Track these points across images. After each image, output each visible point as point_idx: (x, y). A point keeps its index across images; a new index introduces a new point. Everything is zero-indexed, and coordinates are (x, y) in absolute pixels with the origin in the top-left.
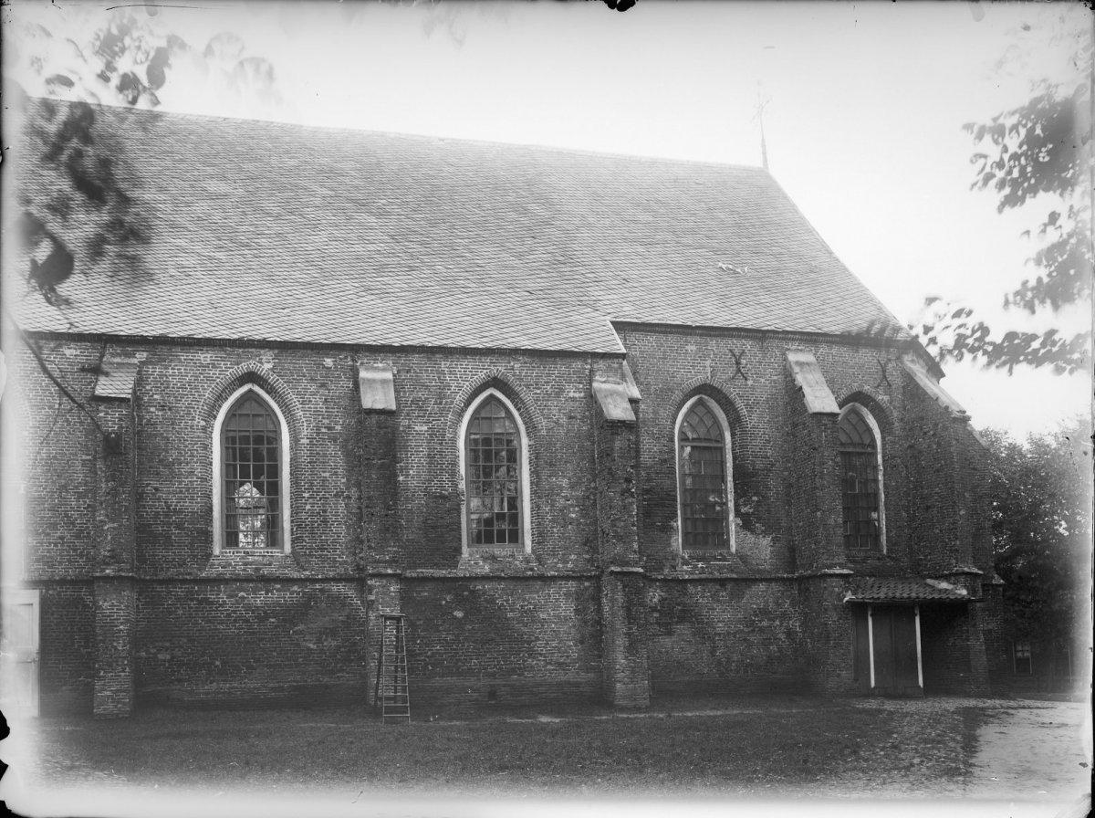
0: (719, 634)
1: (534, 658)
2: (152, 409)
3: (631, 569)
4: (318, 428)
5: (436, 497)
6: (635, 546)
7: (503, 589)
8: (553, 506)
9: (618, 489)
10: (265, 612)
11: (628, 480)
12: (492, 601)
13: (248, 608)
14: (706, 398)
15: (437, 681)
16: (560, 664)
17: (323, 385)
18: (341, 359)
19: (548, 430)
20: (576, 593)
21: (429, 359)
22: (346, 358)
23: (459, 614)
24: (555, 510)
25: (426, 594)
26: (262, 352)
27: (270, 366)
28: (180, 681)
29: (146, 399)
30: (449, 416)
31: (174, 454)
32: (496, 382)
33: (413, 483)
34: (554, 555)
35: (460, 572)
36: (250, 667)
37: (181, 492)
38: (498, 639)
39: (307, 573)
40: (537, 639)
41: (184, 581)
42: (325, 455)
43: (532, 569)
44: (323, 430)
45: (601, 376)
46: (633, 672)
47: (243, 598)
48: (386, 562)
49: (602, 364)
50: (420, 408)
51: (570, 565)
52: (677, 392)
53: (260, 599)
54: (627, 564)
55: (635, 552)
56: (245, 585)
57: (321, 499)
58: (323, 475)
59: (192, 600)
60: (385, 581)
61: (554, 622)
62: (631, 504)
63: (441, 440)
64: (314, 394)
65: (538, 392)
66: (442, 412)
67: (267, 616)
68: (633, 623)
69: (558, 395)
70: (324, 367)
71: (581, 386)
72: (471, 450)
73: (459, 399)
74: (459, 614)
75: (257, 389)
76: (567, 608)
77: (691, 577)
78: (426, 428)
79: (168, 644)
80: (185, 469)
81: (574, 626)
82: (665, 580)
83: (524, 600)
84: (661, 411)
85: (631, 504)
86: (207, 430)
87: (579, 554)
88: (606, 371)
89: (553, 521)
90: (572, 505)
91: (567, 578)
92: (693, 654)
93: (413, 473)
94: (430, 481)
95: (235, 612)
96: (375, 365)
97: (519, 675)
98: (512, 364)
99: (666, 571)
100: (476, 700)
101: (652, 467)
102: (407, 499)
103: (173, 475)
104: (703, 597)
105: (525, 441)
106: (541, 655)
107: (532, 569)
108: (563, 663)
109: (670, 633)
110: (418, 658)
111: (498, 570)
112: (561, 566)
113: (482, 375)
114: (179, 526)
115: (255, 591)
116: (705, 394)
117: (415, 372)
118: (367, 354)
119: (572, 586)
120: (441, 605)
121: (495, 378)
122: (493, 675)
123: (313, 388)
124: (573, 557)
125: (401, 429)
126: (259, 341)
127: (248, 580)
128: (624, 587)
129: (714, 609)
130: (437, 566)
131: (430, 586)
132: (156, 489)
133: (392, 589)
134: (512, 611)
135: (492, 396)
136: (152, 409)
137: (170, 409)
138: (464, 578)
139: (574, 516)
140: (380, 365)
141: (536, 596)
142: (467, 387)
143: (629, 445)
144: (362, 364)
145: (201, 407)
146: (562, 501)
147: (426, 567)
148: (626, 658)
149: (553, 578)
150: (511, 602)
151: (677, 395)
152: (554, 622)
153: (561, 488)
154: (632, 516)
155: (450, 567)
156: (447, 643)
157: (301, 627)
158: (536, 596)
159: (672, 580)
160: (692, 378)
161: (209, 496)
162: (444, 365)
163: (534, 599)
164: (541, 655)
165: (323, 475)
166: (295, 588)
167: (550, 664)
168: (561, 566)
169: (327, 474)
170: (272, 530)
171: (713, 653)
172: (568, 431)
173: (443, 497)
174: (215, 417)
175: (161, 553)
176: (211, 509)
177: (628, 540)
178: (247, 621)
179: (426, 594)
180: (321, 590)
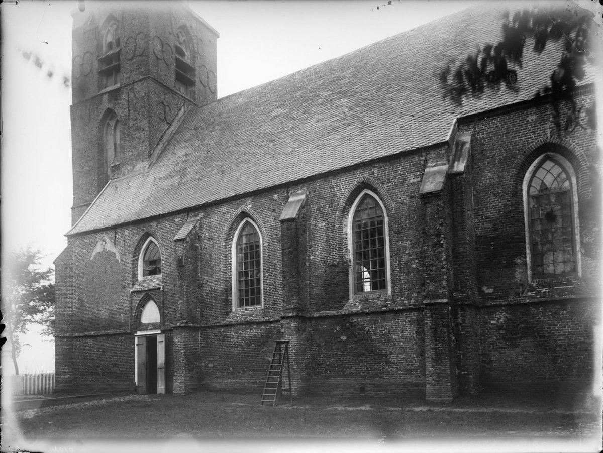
0: (560, 346)
1: (390, 366)
2: (205, 241)
3: (439, 301)
4: (272, 235)
5: (331, 266)
6: (444, 283)
8: (400, 261)
9: (430, 243)
10: (250, 341)
11: (438, 235)
12: (363, 329)
13: (243, 339)
14: (552, 154)
15: (332, 381)
16: (407, 370)
17: (274, 211)
18: (282, 193)
20: (417, 320)
21: (325, 181)
22: (284, 192)
23: (344, 338)
24: (401, 264)
26: (247, 199)
27: (250, 206)
28: (216, 377)
29: (203, 236)
30: (337, 214)
31: (213, 261)
32: (364, 185)
34: (401, 295)
36: (244, 371)
37: (216, 281)
38: (366, 353)
39: (267, 318)
40: (391, 353)
41: (217, 327)
42: (275, 251)
43: (386, 306)
44: (274, 236)
45: (432, 162)
46: (439, 376)
47: (240, 334)
49: (433, 154)
50: (321, 213)
51: (413, 301)
52: (519, 157)
53: (248, 334)
54: (438, 297)
55: (444, 288)
58: (274, 262)
59: (221, 336)
60: (288, 321)
61: (402, 341)
63: (334, 231)
65: (390, 184)
66: (333, 212)
69: (402, 183)
71: (418, 173)
72: (356, 232)
73: (342, 202)
74: (344, 338)
76: (410, 331)
77: (533, 300)
78: (324, 224)
79: (212, 359)
80: (218, 268)
81: (416, 343)
82: (509, 306)
83: (382, 327)
84: (505, 176)
85: (440, 252)
86: (227, 248)
87: (418, 293)
88: (436, 158)
89: (400, 272)
90: (413, 259)
91: (410, 310)
92: (536, 361)
93: (317, 254)
94: (327, 256)
95: (237, 341)
96: (298, 192)
97: (380, 377)
98: (373, 170)
99: (511, 298)
100: (353, 393)
101: (496, 220)
102: (315, 269)
103: (214, 273)
104: (544, 316)
105: (386, 220)
106: (394, 364)
107: (386, 306)
108: (409, 370)
109: (514, 346)
110: (322, 366)
111: (366, 308)
112: (406, 302)
113: (355, 183)
114: (216, 299)
115: (246, 330)
116: (550, 151)
117: (319, 191)
118: (294, 187)
119: (414, 315)
120: (333, 333)
121: (363, 183)
122: (364, 377)
123: (269, 213)
125: (311, 227)
126: (243, 194)
127: (241, 324)
128: (432, 314)
130: (331, 309)
131: (327, 322)
132: (207, 281)
133: (292, 325)
134: (375, 334)
136: (205, 241)
137: (212, 239)
138: (345, 315)
141: (390, 324)
142: (347, 193)
143: (438, 209)
144: (292, 193)
145: (224, 235)
146: (406, 257)
147: (325, 310)
148: (433, 366)
149: (400, 311)
150: (374, 329)
151: (520, 158)
152: (402, 341)
153: (405, 248)
154: (442, 261)
155: (338, 308)
156: (337, 356)
158: (390, 324)
159: (515, 305)
160: (532, 142)
162: (333, 182)
163: (388, 326)
164: (394, 364)
165: (274, 262)
166: (263, 327)
167: (401, 370)
168: (406, 302)
169: (276, 261)
170: (379, 283)
171: (554, 360)
172: (410, 207)
173: (334, 265)
174: (232, 239)
175: (209, 313)
177: (438, 279)
178: (242, 346)
180: (274, 328)
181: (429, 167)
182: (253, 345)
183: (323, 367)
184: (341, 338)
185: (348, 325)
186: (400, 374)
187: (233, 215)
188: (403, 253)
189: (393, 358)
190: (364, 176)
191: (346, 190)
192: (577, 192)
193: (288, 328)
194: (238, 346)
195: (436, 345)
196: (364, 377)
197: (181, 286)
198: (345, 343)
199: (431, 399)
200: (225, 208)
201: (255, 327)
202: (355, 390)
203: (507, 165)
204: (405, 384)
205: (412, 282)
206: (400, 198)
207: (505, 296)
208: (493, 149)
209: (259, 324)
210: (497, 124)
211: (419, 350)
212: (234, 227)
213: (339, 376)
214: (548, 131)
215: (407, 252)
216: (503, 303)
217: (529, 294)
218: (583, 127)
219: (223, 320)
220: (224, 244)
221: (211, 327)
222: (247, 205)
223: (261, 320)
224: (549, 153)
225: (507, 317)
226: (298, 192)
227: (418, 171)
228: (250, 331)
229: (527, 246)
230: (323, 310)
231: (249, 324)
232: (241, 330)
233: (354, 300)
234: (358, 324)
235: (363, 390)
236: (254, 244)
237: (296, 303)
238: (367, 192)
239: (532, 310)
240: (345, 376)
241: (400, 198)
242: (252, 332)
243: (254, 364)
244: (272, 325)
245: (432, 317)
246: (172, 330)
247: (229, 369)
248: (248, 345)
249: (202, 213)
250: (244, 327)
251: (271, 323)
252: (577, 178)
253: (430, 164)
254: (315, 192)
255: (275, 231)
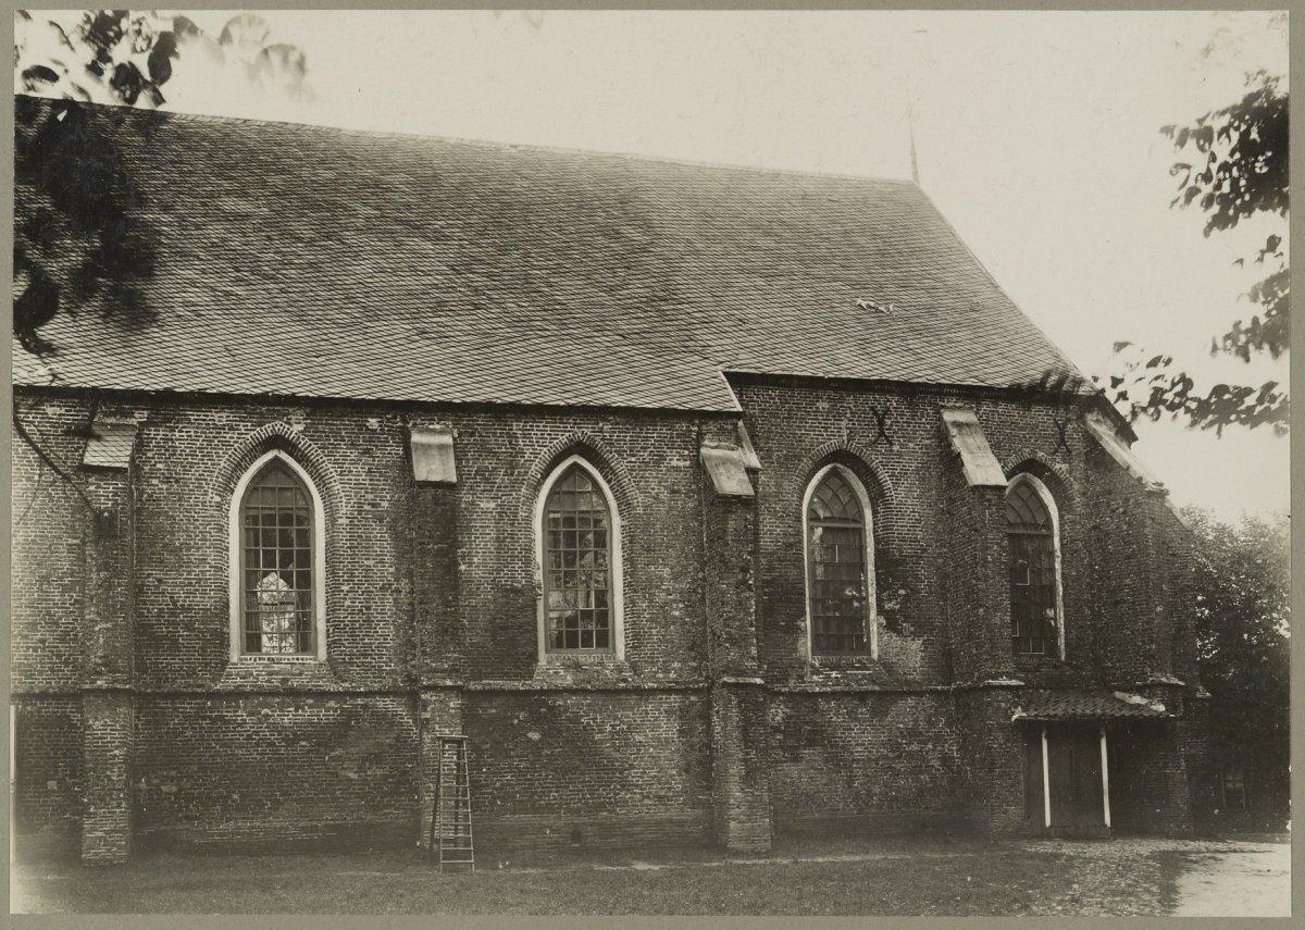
3: (749, 680)
4: (360, 505)
6: (754, 651)
7: (589, 705)
8: (651, 601)
9: (731, 581)
11: (745, 570)
12: (576, 719)
13: (274, 728)
14: (842, 467)
15: (509, 819)
16: (660, 798)
19: (646, 507)
20: (681, 709)
23: (535, 736)
25: (494, 711)
29: (147, 469)
32: (578, 447)
33: (477, 574)
35: (536, 684)
38: (583, 767)
39: (347, 685)
40: (632, 767)
41: (195, 695)
43: (625, 680)
44: (366, 507)
45: (711, 440)
48: (444, 671)
49: (712, 426)
50: (487, 481)
51: (672, 675)
53: (288, 717)
54: (742, 673)
55: (753, 658)
56: (270, 699)
57: (363, 592)
59: (204, 718)
60: (442, 694)
62: (748, 599)
64: (354, 462)
65: (633, 459)
67: (297, 738)
68: (750, 748)
69: (658, 463)
70: (367, 429)
74: (535, 736)
75: (284, 456)
76: (669, 729)
78: (492, 505)
80: (196, 555)
81: (678, 750)
85: (748, 599)
87: (683, 661)
89: (651, 620)
90: (675, 601)
91: (669, 691)
93: (478, 559)
94: (499, 571)
95: (257, 733)
96: (431, 427)
98: (601, 425)
99: (792, 683)
102: (471, 593)
103: (180, 564)
104: (837, 714)
105: (617, 521)
106: (637, 786)
108: (664, 797)
109: (796, 759)
111: (583, 681)
112: (661, 676)
114: (189, 627)
116: (841, 463)
120: (512, 724)
122: (577, 812)
124: (676, 665)
125: (463, 506)
127: (273, 693)
129: (851, 729)
130: (507, 676)
131: (499, 701)
132: (160, 581)
133: (452, 705)
135: (575, 464)
136: (155, 482)
137: (177, 482)
139: (677, 613)
140: (438, 427)
142: (545, 454)
143: (746, 526)
144: (415, 425)
149: (652, 691)
150: (603, 725)
153: (662, 579)
154: (749, 614)
155: (523, 678)
157: (338, 752)
161: (224, 590)
162: (517, 427)
163: (628, 717)
164: (637, 786)
166: (332, 704)
167: (648, 797)
168: (661, 676)
169: (371, 563)
170: (303, 632)
171: (850, 782)
174: (232, 491)
176: (227, 605)
178: (272, 744)
179: (494, 711)
180: (365, 707)
181: (707, 446)
182: (303, 743)
183: (485, 793)
184: (530, 735)
185: (543, 710)
186: (646, 805)
187: (248, 437)
188: (657, 587)
189: (634, 776)
190: (585, 431)
191: (545, 449)
192: (874, 532)
193: (442, 710)
194: (257, 745)
195: (747, 754)
196: (577, 812)
197: (107, 586)
198: (536, 747)
199: (738, 845)
200: (224, 415)
201: (311, 701)
202: (561, 837)
203: (788, 469)
204: (658, 823)
205: (673, 642)
206: (653, 489)
207: (784, 679)
208: (768, 438)
209: (321, 695)
210: (774, 399)
211: (682, 763)
212: (243, 464)
213: (525, 811)
214: (845, 432)
215: (664, 587)
216: (783, 690)
217: (815, 678)
218: (888, 441)
219: (213, 680)
220: (218, 499)
221: (175, 696)
222: (290, 425)
223: (332, 687)
224: (838, 465)
225: (786, 713)
226: (431, 427)
227: (684, 449)
228: (297, 710)
229: (807, 602)
230: (487, 678)
231: (296, 695)
232: (270, 706)
233: (549, 663)
234: (566, 710)
235: (576, 835)
236: (295, 513)
237: (455, 659)
238: (579, 462)
239: (822, 704)
240: (535, 810)
241: (653, 489)
242: (300, 712)
243: (306, 785)
244: (359, 701)
245: (740, 707)
246: (81, 696)
247: (230, 797)
248: (291, 742)
249: (146, 413)
250: (277, 700)
251: (360, 695)
252: (875, 513)
253: (706, 442)
254: (472, 435)
255: (370, 496)
